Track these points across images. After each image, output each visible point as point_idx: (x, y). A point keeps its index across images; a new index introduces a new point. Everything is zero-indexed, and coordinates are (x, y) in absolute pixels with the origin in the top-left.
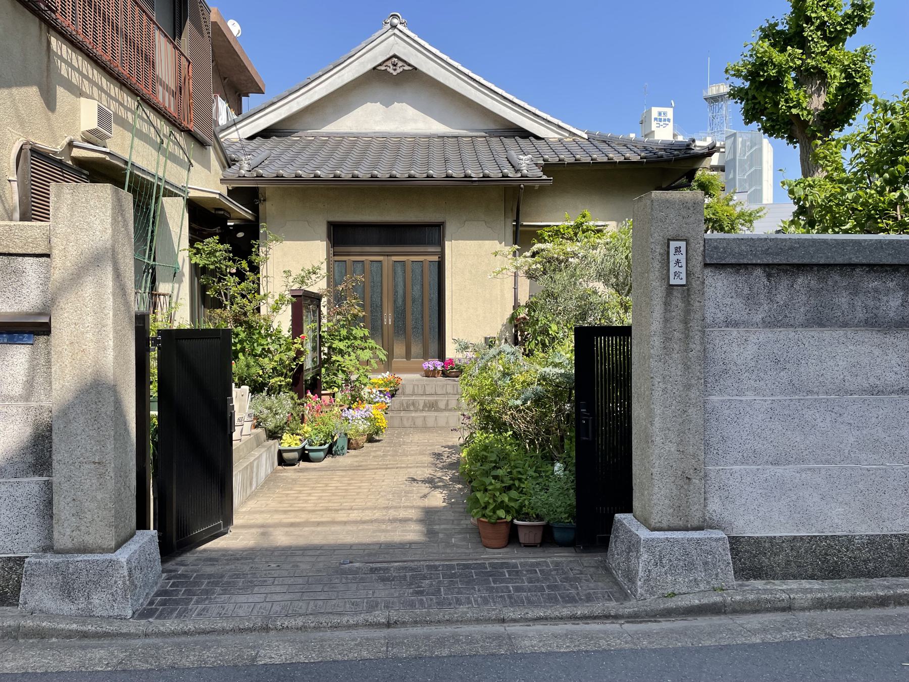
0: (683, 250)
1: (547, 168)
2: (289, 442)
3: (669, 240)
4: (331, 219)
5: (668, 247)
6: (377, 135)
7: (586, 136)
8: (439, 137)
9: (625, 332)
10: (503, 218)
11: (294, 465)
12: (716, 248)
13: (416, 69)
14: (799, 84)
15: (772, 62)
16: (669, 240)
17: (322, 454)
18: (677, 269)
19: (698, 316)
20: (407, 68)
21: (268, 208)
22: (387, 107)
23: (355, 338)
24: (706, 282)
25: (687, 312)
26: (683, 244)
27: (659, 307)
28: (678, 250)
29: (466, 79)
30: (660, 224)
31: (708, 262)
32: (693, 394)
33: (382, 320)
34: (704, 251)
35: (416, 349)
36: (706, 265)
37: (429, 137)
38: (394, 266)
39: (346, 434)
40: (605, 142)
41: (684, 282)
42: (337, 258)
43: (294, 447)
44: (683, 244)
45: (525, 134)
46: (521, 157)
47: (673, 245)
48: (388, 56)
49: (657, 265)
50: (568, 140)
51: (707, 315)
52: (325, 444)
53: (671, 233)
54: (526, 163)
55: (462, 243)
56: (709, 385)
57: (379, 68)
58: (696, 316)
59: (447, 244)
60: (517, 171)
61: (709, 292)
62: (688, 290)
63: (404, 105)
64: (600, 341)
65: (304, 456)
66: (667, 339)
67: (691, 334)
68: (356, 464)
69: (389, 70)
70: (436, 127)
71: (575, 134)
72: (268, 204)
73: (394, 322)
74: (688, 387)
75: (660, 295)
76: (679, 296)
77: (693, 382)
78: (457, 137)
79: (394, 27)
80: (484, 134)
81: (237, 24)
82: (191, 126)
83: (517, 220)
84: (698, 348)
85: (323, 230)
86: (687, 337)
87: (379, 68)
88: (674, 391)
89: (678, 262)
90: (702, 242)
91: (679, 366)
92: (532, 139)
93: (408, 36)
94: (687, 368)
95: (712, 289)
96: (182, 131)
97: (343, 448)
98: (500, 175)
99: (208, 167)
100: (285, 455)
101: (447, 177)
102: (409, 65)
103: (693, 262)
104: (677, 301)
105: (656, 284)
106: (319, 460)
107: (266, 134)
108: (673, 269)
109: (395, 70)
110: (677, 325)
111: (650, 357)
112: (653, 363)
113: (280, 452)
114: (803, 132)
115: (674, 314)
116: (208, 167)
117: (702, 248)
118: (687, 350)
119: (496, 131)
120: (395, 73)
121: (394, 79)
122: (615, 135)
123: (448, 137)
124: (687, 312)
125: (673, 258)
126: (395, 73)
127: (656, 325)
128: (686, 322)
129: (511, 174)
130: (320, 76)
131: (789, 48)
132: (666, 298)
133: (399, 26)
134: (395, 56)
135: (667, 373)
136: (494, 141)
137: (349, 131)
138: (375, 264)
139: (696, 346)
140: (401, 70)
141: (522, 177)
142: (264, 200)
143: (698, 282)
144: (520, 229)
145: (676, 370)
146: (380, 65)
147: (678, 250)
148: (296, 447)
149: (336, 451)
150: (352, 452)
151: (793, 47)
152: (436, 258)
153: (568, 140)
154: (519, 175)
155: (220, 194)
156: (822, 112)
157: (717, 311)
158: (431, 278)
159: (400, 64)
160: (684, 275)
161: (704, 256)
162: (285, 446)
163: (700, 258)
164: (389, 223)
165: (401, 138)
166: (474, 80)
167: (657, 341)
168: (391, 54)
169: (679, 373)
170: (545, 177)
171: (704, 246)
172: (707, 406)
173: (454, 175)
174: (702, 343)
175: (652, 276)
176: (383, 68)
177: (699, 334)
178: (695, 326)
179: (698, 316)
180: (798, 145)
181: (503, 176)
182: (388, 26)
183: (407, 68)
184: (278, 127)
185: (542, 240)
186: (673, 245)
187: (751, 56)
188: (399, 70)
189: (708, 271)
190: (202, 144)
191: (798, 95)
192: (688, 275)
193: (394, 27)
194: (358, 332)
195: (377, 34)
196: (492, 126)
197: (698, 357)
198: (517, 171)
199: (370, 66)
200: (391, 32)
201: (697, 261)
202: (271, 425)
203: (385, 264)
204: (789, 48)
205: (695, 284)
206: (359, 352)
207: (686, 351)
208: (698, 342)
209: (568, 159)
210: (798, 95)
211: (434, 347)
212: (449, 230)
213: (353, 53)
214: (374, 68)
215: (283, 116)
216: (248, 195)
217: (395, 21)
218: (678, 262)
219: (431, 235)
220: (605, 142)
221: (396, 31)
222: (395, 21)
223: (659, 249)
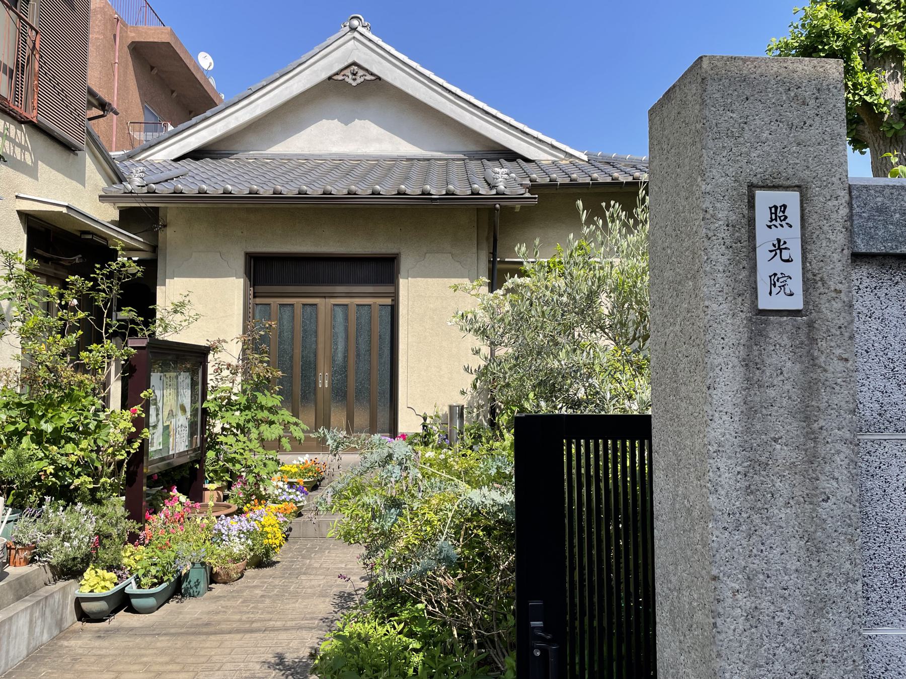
0: (793, 214)
1: (534, 187)
2: (97, 583)
3: (752, 187)
4: (251, 249)
5: (751, 205)
6: (334, 157)
7: (586, 158)
8: (408, 160)
9: (637, 428)
10: (475, 250)
11: (104, 620)
12: (881, 210)
13: (379, 78)
14: (868, 69)
15: (834, 33)
16: (752, 187)
17: (152, 601)
18: (778, 266)
19: (840, 399)
20: (369, 77)
21: (171, 236)
22: (346, 124)
23: (262, 408)
24: (857, 305)
25: (810, 388)
26: (791, 199)
27: (728, 373)
28: (778, 213)
29: (439, 90)
30: (729, 143)
31: (862, 248)
32: (834, 625)
33: (316, 382)
34: (850, 217)
35: (361, 418)
36: (858, 258)
37: (395, 159)
38: (333, 310)
39: (203, 564)
40: (609, 163)
41: (796, 303)
42: (258, 301)
43: (98, 592)
44: (791, 199)
45: (512, 156)
46: (497, 170)
47: (765, 199)
48: (346, 64)
49: (720, 256)
50: (564, 162)
51: (865, 396)
52: (160, 583)
53: (758, 169)
54: (503, 177)
55: (421, 281)
56: (874, 596)
57: (336, 77)
58: (835, 400)
59: (402, 282)
60: (491, 186)
61: (868, 332)
62: (811, 325)
63: (367, 123)
64: (573, 450)
65: (123, 602)
66: (755, 464)
67: (822, 450)
68: (206, 618)
69: (347, 79)
70: (407, 149)
71: (571, 156)
72: (169, 231)
73: (331, 383)
74: (819, 605)
75: (731, 339)
76: (786, 341)
77: (834, 589)
78: (428, 160)
79: (353, 29)
80: (462, 156)
81: (209, 57)
82: (32, 115)
83: (494, 254)
84: (845, 490)
85: (239, 263)
86: (812, 459)
87: (336, 77)
88: (780, 617)
89: (779, 247)
90: (844, 195)
91: (793, 544)
92: (520, 161)
93: (370, 40)
94: (815, 548)
95: (875, 324)
96: (21, 122)
97: (197, 583)
98: (469, 192)
99: (81, 180)
100: (85, 606)
101: (399, 194)
102: (372, 74)
103: (821, 248)
104: (780, 357)
105: (720, 307)
106: (149, 611)
107: (196, 155)
108: (766, 266)
109: (354, 80)
110: (786, 427)
111: (707, 515)
112: (717, 536)
113: (78, 601)
114: (876, 130)
115: (772, 393)
116: (81, 180)
117: (844, 211)
118: (814, 498)
119: (477, 152)
120: (354, 84)
121: (354, 90)
122: (622, 156)
123: (419, 160)
124: (810, 388)
125: (765, 237)
126: (354, 84)
127: (723, 427)
128: (806, 415)
129: (484, 190)
130: (264, 87)
131: (860, 10)
132: (749, 348)
133: (360, 29)
134: (354, 64)
135: (757, 564)
136: (474, 165)
137: (298, 151)
138: (309, 309)
139: (838, 485)
140: (362, 79)
141: (497, 194)
142: (165, 226)
143: (837, 305)
144: (498, 266)
145: (785, 557)
146: (337, 74)
147: (778, 213)
148: (105, 593)
149: (187, 589)
150: (218, 588)
151: (864, 9)
152: (388, 301)
153: (564, 162)
154: (494, 192)
155: (67, 207)
156: (901, 103)
157: (891, 386)
158: (380, 327)
159: (361, 72)
160: (796, 285)
161: (851, 232)
162: (85, 591)
163: (840, 238)
164: (325, 259)
165: (360, 160)
166: (450, 91)
167: (726, 471)
168: (350, 61)
169: (793, 565)
170: (528, 195)
171: (850, 205)
172: (871, 656)
173: (408, 192)
174: (852, 478)
175: (707, 286)
176: (340, 77)
177: (846, 450)
178: (834, 428)
179: (840, 399)
180: (868, 150)
181: (473, 194)
182: (347, 29)
183: (369, 77)
184: (214, 148)
185: (523, 274)
186: (765, 199)
187: (803, 26)
188: (359, 80)
189: (862, 274)
190: (69, 148)
191: (869, 79)
192: (810, 282)
193: (353, 29)
194: (269, 400)
195: (333, 38)
196: (472, 147)
197: (845, 518)
198: (491, 186)
199: (324, 76)
200: (350, 35)
201: (834, 246)
202: (56, 557)
203: (321, 308)
204: (860, 10)
205: (830, 311)
206: (264, 427)
207: (809, 498)
208: (842, 474)
209: (561, 179)
210: (869, 79)
211: (383, 418)
212: (405, 264)
213: (304, 59)
214: (330, 78)
215: (218, 133)
216: (141, 217)
217: (355, 23)
218: (779, 247)
219: (383, 271)
220: (609, 163)
221: (356, 35)
222: (355, 23)
223: (724, 212)
